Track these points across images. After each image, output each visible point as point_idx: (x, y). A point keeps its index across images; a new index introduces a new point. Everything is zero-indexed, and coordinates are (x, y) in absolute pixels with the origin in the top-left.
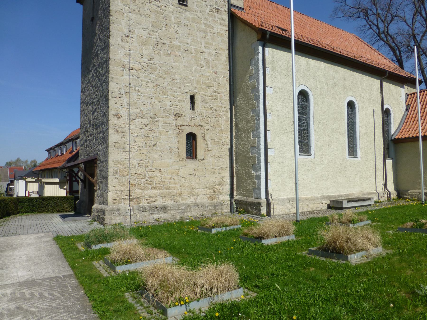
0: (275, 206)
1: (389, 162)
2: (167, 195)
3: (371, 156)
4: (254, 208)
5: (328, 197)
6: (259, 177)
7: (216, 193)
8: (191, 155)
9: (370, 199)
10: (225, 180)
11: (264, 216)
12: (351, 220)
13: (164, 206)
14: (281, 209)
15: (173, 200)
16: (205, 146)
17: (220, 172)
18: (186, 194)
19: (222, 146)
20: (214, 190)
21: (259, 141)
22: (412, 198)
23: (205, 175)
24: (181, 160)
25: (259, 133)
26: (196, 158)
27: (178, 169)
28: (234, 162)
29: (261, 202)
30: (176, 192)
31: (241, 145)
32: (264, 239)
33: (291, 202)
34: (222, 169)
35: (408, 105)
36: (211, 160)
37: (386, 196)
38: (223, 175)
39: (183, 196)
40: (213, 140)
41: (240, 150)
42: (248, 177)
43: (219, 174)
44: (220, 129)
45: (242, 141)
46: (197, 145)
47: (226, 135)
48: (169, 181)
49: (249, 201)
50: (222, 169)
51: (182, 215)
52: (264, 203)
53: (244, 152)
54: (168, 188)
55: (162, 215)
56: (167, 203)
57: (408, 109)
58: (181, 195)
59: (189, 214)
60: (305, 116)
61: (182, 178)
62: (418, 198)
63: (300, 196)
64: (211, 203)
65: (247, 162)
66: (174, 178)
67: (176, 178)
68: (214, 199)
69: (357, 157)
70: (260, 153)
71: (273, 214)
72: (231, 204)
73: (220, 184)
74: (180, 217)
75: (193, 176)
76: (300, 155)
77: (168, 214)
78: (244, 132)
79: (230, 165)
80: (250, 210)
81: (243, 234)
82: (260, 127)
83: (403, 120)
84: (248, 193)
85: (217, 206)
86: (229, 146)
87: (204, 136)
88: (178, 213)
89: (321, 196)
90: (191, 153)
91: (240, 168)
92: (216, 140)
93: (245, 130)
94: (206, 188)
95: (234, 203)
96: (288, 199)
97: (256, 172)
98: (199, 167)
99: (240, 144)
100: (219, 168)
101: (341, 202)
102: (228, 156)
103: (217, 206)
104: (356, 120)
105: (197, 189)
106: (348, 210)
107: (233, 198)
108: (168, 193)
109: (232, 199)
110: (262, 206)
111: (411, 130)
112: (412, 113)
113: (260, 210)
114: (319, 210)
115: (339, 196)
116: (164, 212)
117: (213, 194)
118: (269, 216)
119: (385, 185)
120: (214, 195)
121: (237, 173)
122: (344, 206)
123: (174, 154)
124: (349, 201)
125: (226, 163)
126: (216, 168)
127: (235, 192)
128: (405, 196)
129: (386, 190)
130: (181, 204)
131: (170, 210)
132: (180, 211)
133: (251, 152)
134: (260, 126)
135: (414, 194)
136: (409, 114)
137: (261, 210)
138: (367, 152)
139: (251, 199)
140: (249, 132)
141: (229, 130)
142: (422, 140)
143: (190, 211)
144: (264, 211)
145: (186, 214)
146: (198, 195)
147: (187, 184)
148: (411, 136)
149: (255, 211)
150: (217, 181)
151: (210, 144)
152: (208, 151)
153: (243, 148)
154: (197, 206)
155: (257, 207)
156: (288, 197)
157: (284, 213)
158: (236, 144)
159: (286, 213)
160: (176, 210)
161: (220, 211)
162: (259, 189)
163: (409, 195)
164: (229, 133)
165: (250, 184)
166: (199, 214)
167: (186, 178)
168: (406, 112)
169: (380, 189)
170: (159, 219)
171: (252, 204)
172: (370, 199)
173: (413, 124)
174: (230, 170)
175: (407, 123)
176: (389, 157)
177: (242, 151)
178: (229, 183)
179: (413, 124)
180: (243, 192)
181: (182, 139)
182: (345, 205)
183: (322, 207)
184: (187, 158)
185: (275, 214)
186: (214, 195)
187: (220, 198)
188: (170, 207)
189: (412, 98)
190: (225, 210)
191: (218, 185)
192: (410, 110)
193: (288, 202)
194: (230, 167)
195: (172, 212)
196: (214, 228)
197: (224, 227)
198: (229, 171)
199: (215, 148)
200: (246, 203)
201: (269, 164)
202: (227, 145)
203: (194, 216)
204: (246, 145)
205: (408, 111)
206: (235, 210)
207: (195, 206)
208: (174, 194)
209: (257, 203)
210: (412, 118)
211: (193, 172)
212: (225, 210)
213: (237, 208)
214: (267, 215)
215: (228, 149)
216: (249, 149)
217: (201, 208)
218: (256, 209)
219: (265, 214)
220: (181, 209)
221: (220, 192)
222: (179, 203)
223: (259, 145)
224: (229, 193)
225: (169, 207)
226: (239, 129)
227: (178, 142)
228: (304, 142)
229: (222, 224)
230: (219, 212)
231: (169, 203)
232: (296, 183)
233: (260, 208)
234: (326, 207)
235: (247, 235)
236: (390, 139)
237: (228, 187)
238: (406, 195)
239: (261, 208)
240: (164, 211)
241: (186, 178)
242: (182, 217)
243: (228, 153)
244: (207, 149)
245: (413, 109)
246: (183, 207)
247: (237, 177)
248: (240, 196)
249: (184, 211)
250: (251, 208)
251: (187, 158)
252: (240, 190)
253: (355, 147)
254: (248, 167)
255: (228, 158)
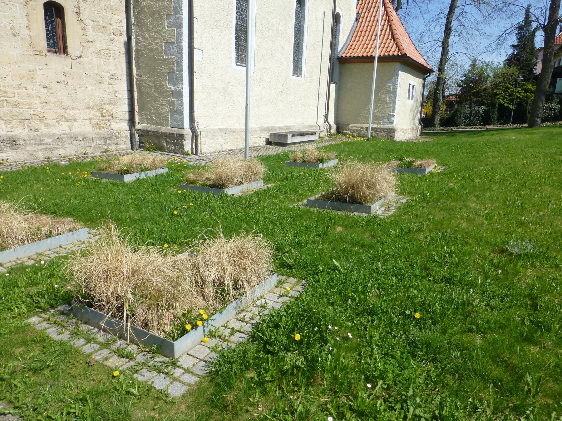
0: (203, 140)
1: (333, 86)
2: (14, 118)
3: (316, 77)
4: (171, 143)
5: (267, 129)
6: (179, 94)
7: (106, 118)
8: (54, 46)
9: (314, 133)
10: (120, 96)
11: (189, 155)
12: (321, 158)
13: (12, 137)
14: (211, 145)
15: (28, 126)
16: (82, 32)
17: (111, 81)
18: (52, 118)
19: (113, 36)
20: (102, 112)
21: (180, 34)
22: (352, 133)
23: (86, 86)
24: (38, 53)
25: (180, 19)
26: (65, 51)
27: (34, 71)
28: (134, 67)
29: (183, 133)
30: (32, 113)
31: (146, 39)
32: (228, 187)
33: (223, 134)
34: (114, 78)
35: (358, 13)
36: (94, 59)
37: (326, 131)
38: (116, 87)
39: (46, 121)
40: (96, 23)
41: (145, 46)
42: (159, 94)
43: (109, 86)
44: (107, 4)
45: (148, 31)
46: (67, 27)
47: (119, 18)
48: (17, 91)
49: (163, 131)
50: (114, 78)
51: (48, 154)
52: (188, 134)
53: (151, 50)
54: (15, 105)
55: (9, 155)
56: (16, 131)
57: (358, 18)
58: (42, 119)
59: (62, 152)
60: (244, 3)
61: (41, 87)
62: (359, 133)
63: (251, 125)
64: (98, 134)
65: (157, 69)
66: (25, 86)
67: (30, 86)
68: (103, 127)
69: (301, 77)
70: (181, 54)
71: (201, 151)
72: (132, 136)
73: (112, 103)
74: (45, 157)
75: (62, 85)
76: (237, 65)
77: (21, 153)
78: (151, 16)
79: (127, 72)
80: (165, 145)
81: (187, 181)
82: (181, 10)
83: (352, 33)
84: (160, 119)
85: (110, 138)
86: (124, 38)
87: (78, 11)
88: (41, 150)
89: (259, 127)
90: (54, 43)
91: (144, 77)
92: (102, 23)
93: (154, 12)
94: (89, 108)
95: (137, 135)
96: (220, 129)
97: (174, 85)
98: (73, 70)
99: (144, 37)
100: (109, 75)
101: (285, 136)
102: (124, 55)
103: (110, 138)
104: (304, 23)
105: (73, 108)
106: (293, 146)
107: (134, 126)
108: (17, 114)
109: (133, 128)
110: (185, 140)
111: (361, 47)
112: (362, 25)
113: (182, 146)
114: (257, 147)
115: (280, 128)
116: (12, 148)
117: (101, 118)
118: (195, 154)
119: (327, 116)
120: (103, 120)
121: (139, 86)
122: (288, 142)
123: (22, 39)
124: (295, 135)
125: (120, 68)
126: (103, 74)
127: (137, 117)
128: (345, 131)
129: (327, 123)
130: (46, 135)
131: (25, 144)
132: (45, 146)
133: (166, 51)
134: (183, 8)
135: (355, 128)
136: (359, 25)
137: (185, 146)
138: (313, 70)
139: (166, 129)
140: (161, 17)
141: (124, 9)
142: (378, 62)
143: (63, 147)
144: (188, 147)
145: (56, 152)
146: (75, 120)
147: (52, 99)
148: (360, 55)
149: (173, 148)
150: (106, 97)
151: (91, 29)
152: (88, 41)
153: (150, 44)
154: (75, 138)
155: (177, 140)
156: (220, 127)
157: (215, 150)
158: (136, 35)
159: (217, 150)
160: (35, 144)
161: (114, 146)
162: (181, 113)
163: (349, 129)
164: (124, 15)
165: (164, 105)
166: (79, 152)
167: (50, 89)
168: (356, 23)
169: (321, 122)
170: (5, 162)
171: (168, 136)
172: (314, 133)
173: (355, 40)
174: (127, 81)
175: (356, 37)
176: (332, 81)
177: (147, 49)
178: (126, 101)
179: (355, 40)
180: (151, 117)
181: (35, 12)
182: (290, 140)
183: (259, 142)
184: (49, 51)
185: (202, 152)
186: (103, 120)
187: (112, 127)
188: (24, 140)
189: (363, 5)
190: (122, 146)
191: (108, 104)
192: (360, 20)
193: (221, 134)
194: (127, 76)
195: (28, 149)
196: (127, 173)
197: (142, 171)
198: (126, 82)
199: (100, 38)
200: (158, 135)
201: (195, 73)
202: (121, 35)
203: (71, 155)
204: (156, 38)
205: (357, 21)
206: (138, 146)
207: (71, 138)
208: (28, 117)
209: (177, 134)
210: (362, 32)
211: (63, 78)
212: (122, 146)
213: (141, 142)
214: (192, 153)
215: (123, 43)
216: (162, 46)
217: (82, 142)
218: (175, 144)
219: (190, 152)
220: (46, 144)
221: (112, 116)
222: (41, 133)
223: (180, 41)
224: (127, 118)
225: (21, 139)
226: (142, 8)
227: (27, 16)
228: (241, 45)
229: (139, 167)
230: (113, 149)
231: (20, 132)
232: (247, 105)
233: (182, 142)
234: (265, 143)
235: (193, 182)
236: (336, 56)
237: (126, 108)
238: (346, 129)
239: (184, 142)
240: (12, 146)
241: (50, 89)
242: (49, 158)
243: (123, 50)
244: (86, 37)
245: (364, 20)
246: (50, 141)
247: (140, 92)
248: (146, 123)
249: (51, 146)
250: (167, 142)
251: (49, 51)
252: (146, 115)
253: (299, 62)
254: (160, 76)
255: (123, 59)
